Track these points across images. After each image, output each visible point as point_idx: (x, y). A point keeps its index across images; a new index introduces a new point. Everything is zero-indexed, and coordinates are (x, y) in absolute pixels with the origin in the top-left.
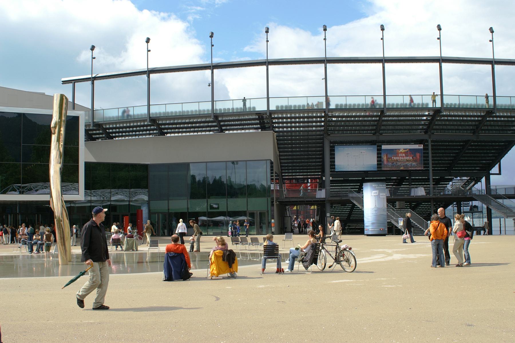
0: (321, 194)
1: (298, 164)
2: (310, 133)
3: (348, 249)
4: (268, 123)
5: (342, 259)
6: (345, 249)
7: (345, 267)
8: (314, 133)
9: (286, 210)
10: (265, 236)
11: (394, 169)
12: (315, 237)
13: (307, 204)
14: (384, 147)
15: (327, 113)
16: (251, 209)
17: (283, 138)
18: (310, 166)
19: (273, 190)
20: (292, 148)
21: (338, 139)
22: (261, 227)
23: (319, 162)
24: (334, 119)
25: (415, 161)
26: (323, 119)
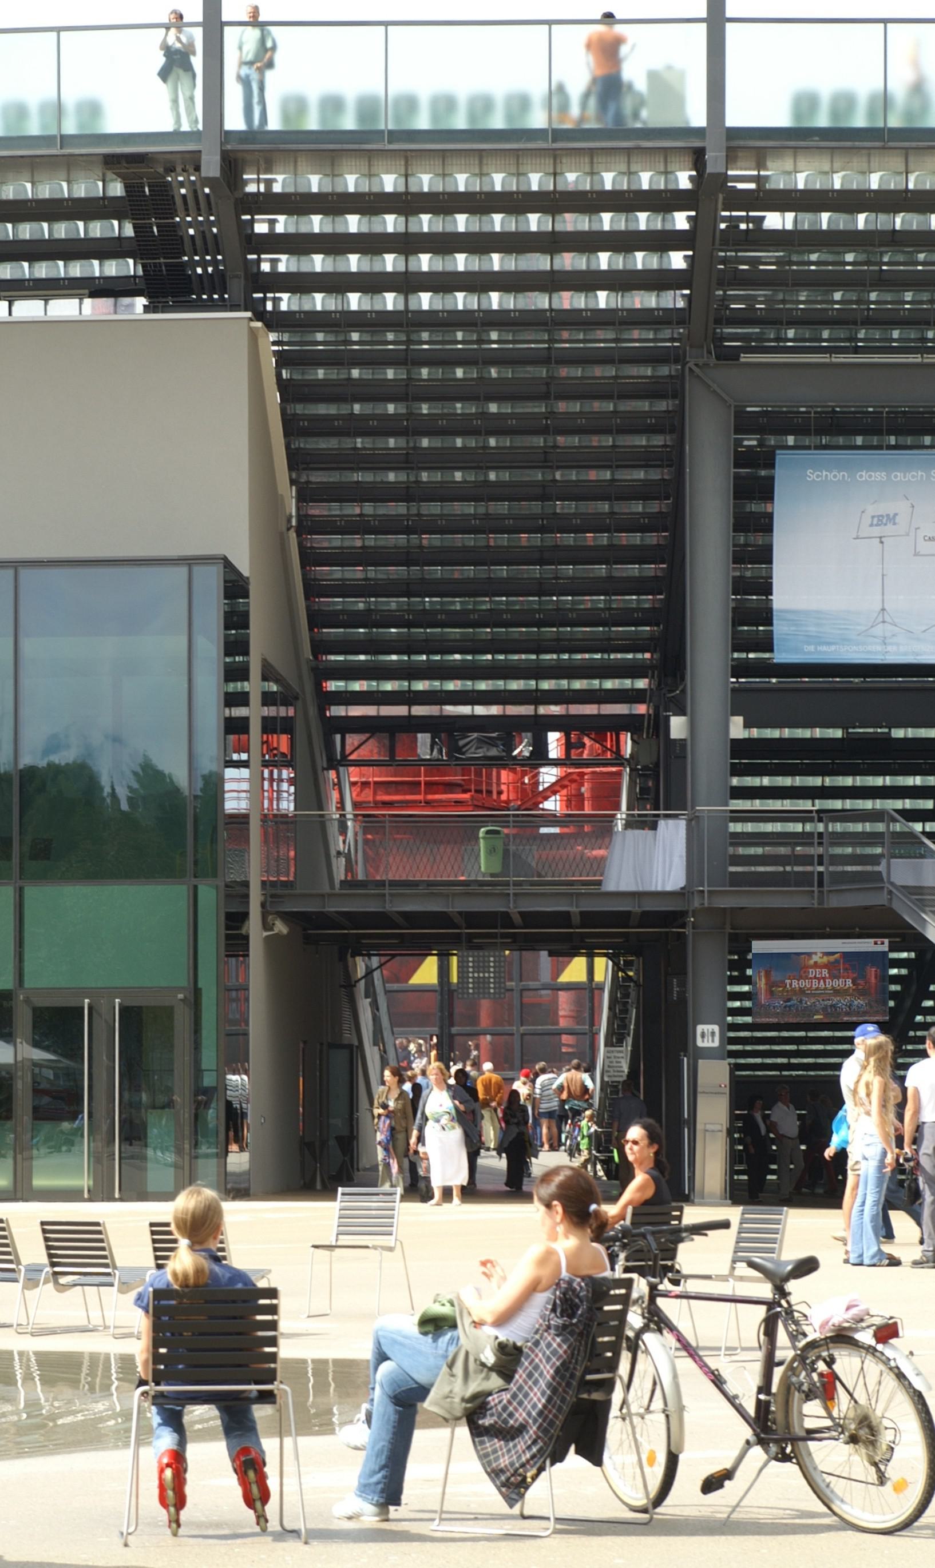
0: (653, 860)
1: (457, 604)
2: (568, 340)
3: (866, 1337)
4: (208, 244)
5: (813, 1413)
6: (842, 1337)
7: (838, 1486)
8: (602, 339)
9: (350, 985)
10: (164, 1211)
11: (791, 1020)
12: (600, 1230)
13: (529, 943)
14: (759, 946)
15: (714, 161)
16: (48, 975)
17: (334, 374)
18: (560, 618)
19: (241, 820)
20: (408, 461)
21: (805, 397)
22: (134, 1133)
23: (639, 586)
24: (774, 221)
25: (862, 993)
26: (681, 221)
